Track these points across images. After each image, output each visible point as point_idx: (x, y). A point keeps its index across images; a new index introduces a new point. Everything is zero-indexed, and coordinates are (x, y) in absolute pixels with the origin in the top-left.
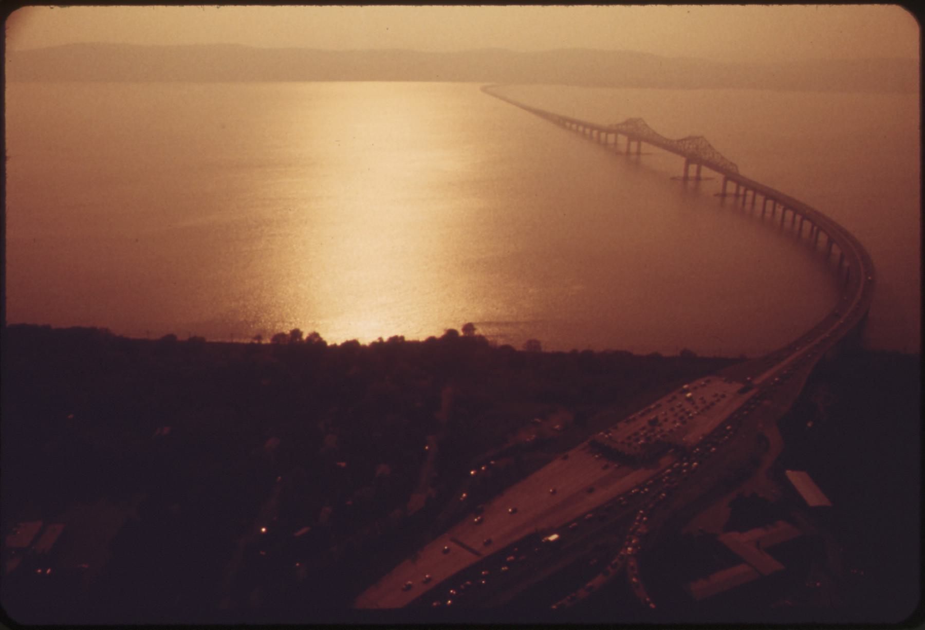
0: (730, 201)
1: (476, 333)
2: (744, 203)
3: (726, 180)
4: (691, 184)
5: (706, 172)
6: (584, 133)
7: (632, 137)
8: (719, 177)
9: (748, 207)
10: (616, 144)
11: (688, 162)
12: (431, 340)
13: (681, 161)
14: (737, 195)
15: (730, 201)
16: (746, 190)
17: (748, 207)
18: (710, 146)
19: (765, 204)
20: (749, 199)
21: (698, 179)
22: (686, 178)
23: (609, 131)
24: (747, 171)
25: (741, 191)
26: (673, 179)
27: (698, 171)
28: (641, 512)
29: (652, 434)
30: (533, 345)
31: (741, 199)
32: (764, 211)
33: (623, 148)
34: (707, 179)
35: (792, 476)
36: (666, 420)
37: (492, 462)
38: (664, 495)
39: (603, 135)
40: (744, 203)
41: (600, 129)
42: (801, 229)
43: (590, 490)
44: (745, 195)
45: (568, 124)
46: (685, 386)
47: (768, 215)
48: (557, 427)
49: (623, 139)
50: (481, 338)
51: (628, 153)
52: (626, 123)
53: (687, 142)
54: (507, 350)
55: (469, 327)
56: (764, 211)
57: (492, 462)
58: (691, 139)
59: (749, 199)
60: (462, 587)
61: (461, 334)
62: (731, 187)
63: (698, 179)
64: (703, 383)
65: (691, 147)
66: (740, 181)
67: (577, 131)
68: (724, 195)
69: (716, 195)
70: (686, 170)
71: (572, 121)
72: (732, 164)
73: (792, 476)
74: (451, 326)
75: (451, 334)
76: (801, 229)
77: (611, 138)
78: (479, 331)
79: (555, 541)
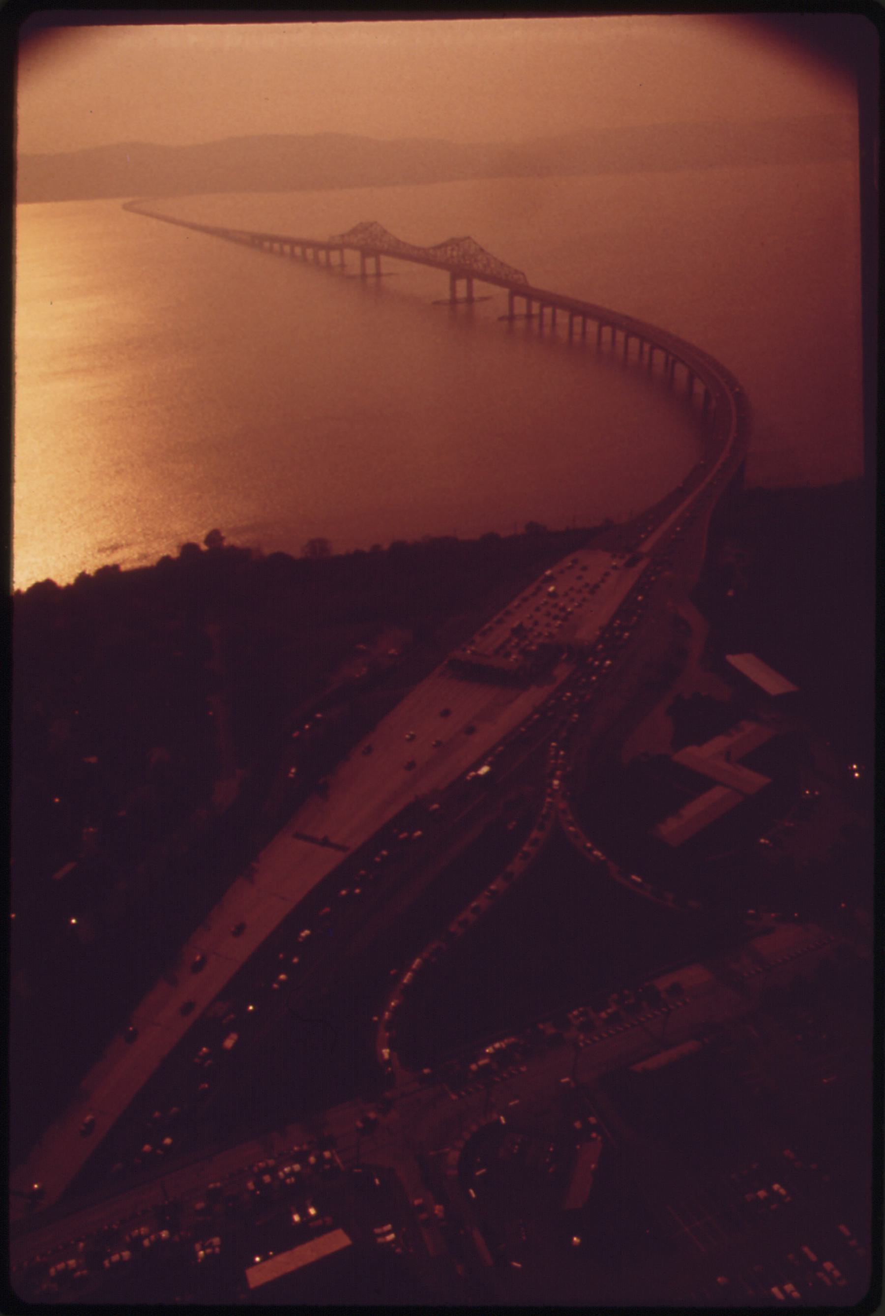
0: (520, 324)
1: (225, 544)
2: (541, 325)
3: (512, 296)
4: (462, 308)
5: (481, 288)
6: (293, 255)
7: (366, 252)
8: (500, 293)
9: (547, 330)
10: (343, 265)
11: (454, 278)
12: (166, 561)
13: (444, 276)
14: (529, 316)
15: (520, 324)
16: (542, 307)
17: (547, 330)
18: (482, 250)
19: (571, 325)
20: (548, 319)
21: (470, 300)
22: (454, 301)
23: (328, 247)
24: (537, 281)
25: (536, 309)
26: (437, 303)
27: (470, 288)
28: (554, 744)
29: (527, 642)
30: (318, 546)
31: (536, 323)
32: (571, 333)
33: (356, 270)
34: (484, 299)
35: (735, 660)
36: (536, 623)
37: (319, 715)
38: (576, 716)
39: (335, 256)
40: (541, 325)
41: (317, 246)
42: (626, 352)
43: (470, 730)
44: (541, 315)
45: (267, 244)
46: (548, 572)
47: (577, 338)
48: (392, 651)
49: (352, 257)
50: (233, 548)
51: (364, 276)
52: (354, 231)
53: (449, 248)
54: (280, 560)
55: (214, 537)
56: (571, 333)
57: (319, 715)
58: (455, 242)
59: (548, 319)
60: (378, 859)
61: (204, 547)
62: (520, 305)
63: (470, 300)
64: (570, 564)
65: (455, 253)
66: (531, 294)
67: (282, 253)
68: (511, 318)
69: (501, 319)
70: (453, 288)
71: (273, 239)
72: (516, 272)
73: (735, 660)
74: (187, 538)
75: (189, 549)
76: (626, 352)
77: (335, 256)
78: (230, 540)
79: (487, 774)
